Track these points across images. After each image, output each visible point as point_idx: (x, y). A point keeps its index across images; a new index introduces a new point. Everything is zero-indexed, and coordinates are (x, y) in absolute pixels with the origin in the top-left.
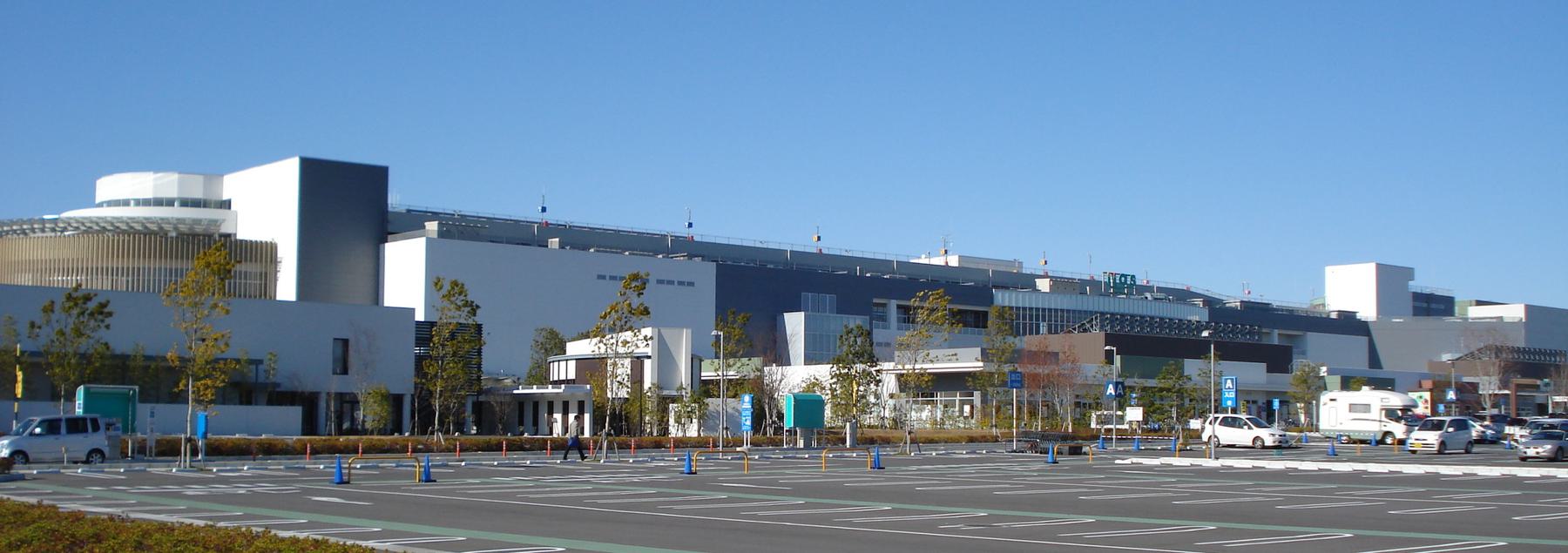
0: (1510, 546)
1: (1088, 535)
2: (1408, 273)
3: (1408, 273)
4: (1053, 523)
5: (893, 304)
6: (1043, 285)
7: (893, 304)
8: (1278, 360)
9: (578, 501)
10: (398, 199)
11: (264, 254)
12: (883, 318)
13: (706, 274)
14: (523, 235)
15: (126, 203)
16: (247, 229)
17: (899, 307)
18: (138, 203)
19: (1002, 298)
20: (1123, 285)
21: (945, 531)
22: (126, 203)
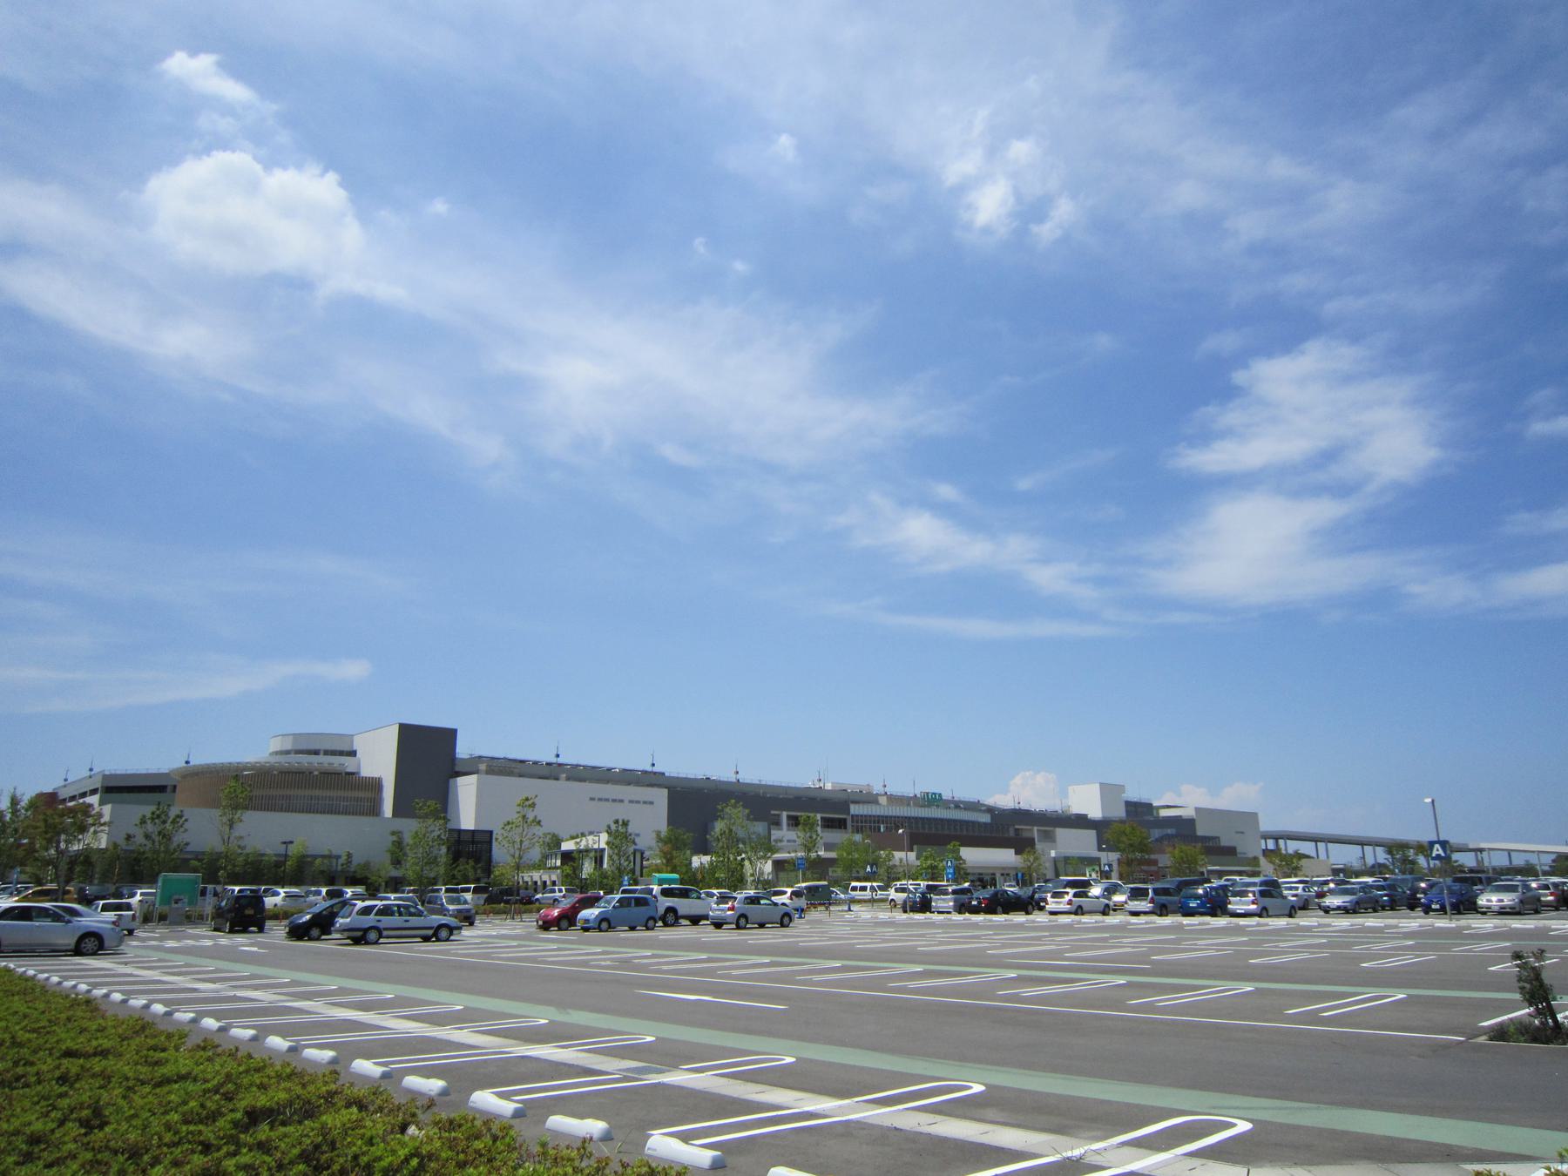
0: (1129, 985)
1: (816, 978)
2: (1121, 788)
3: (1121, 788)
4: (882, 972)
5: (784, 814)
6: (883, 800)
7: (784, 814)
8: (1022, 845)
9: (585, 964)
10: (463, 750)
11: (375, 785)
12: (777, 824)
13: (661, 797)
14: (551, 771)
15: (316, 753)
16: (367, 772)
17: (789, 817)
18: (327, 753)
19: (855, 809)
20: (933, 800)
21: (721, 977)
22: (316, 753)
